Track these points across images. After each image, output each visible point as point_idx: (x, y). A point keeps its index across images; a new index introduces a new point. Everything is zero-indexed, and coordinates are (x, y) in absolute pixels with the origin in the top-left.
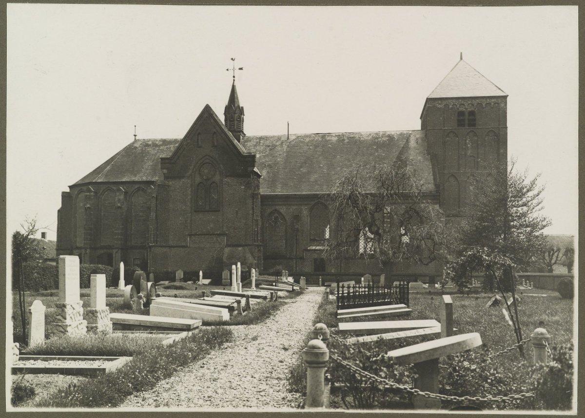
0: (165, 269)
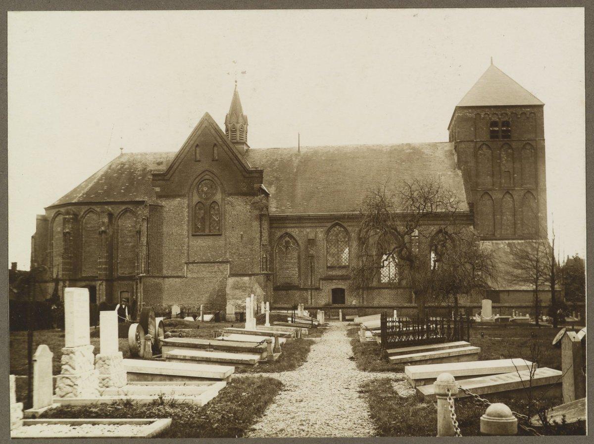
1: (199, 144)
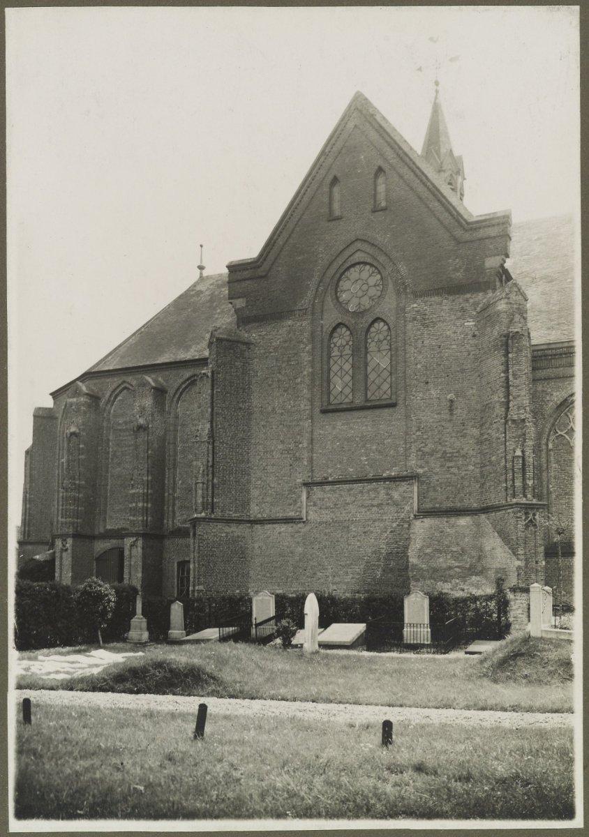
0: (239, 587)
1: (339, 175)
